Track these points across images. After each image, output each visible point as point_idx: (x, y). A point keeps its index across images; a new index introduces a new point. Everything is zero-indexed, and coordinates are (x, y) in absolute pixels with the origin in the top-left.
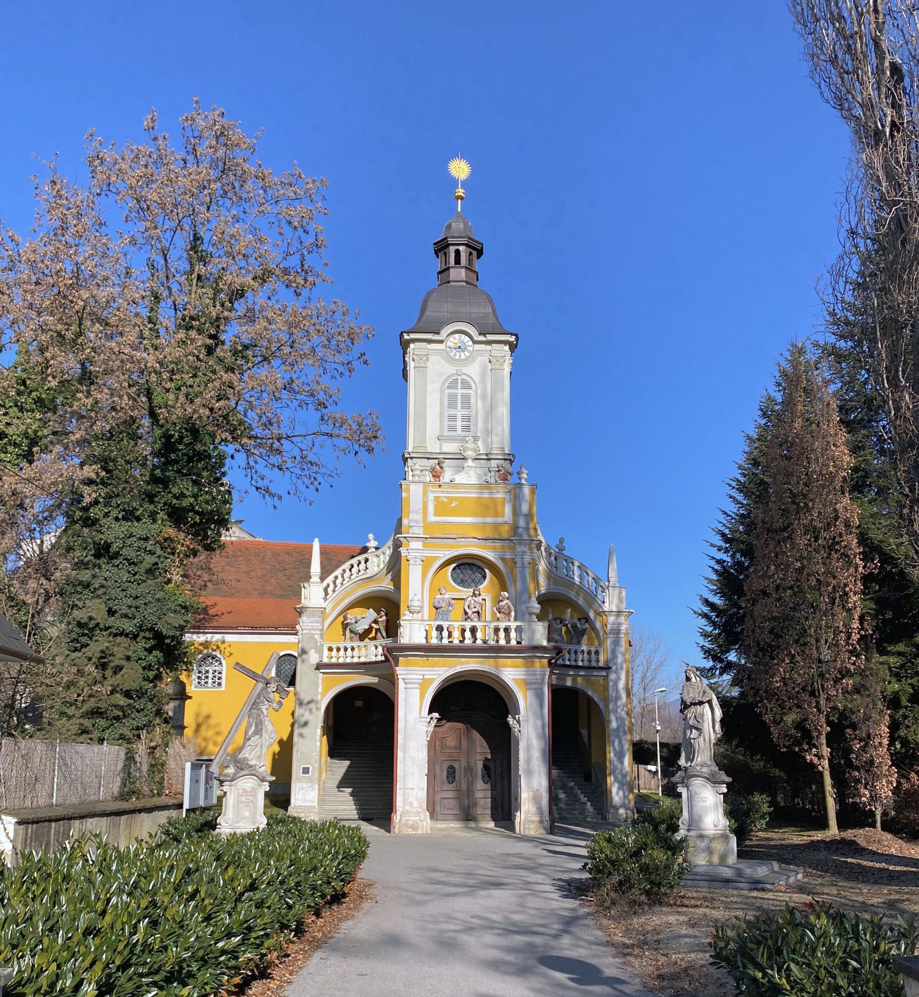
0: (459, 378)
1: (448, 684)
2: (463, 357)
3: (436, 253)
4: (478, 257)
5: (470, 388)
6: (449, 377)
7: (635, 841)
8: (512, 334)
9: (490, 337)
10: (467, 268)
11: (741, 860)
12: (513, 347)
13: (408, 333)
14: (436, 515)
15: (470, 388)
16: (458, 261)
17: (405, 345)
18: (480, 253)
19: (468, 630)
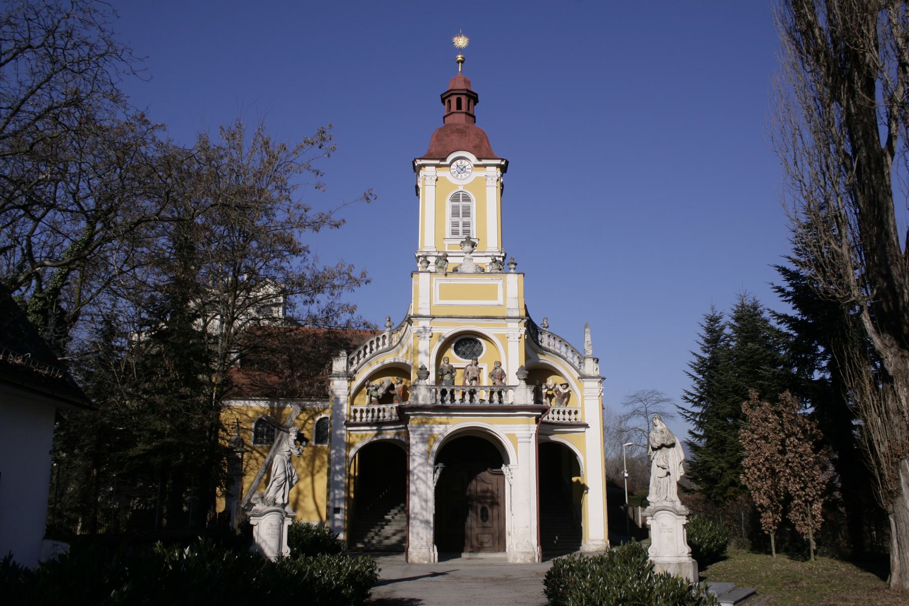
8: (503, 160)
16: (459, 106)
18: (476, 101)
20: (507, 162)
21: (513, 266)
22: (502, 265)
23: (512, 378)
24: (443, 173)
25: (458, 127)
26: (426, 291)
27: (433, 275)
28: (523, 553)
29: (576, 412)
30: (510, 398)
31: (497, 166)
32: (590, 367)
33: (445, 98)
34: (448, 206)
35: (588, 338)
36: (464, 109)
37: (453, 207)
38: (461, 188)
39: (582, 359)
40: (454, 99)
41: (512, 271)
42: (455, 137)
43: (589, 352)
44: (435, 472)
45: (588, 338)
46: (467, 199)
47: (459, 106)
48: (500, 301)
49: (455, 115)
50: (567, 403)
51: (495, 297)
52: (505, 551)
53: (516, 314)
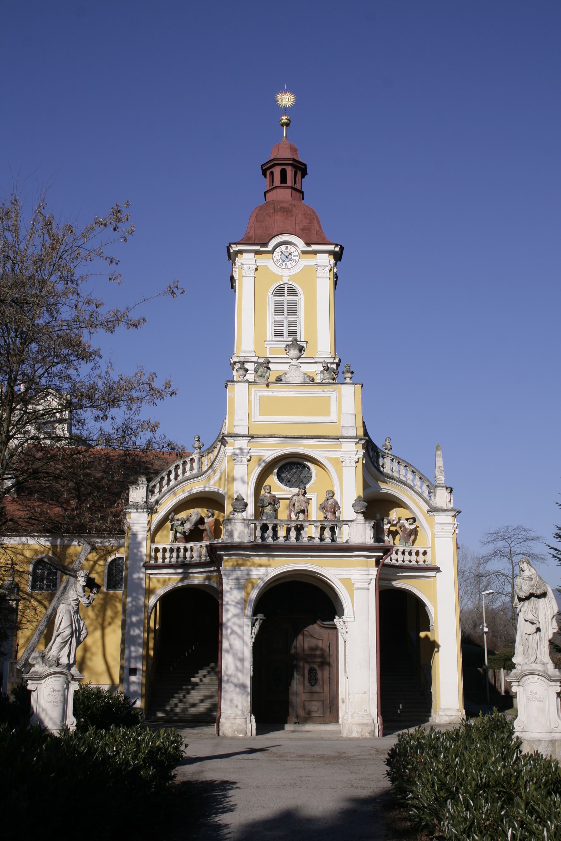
0: (286, 286)
1: (268, 588)
2: (289, 266)
3: (264, 173)
4: (303, 177)
5: (296, 295)
6: (273, 160)
7: (519, 783)
8: (336, 245)
9: (314, 248)
10: (293, 188)
11: (199, 517)
12: (338, 256)
13: (236, 244)
14: (261, 414)
15: (296, 295)
16: (284, 180)
17: (232, 257)
18: (304, 173)
19: (293, 529)
20: (342, 248)
21: (349, 375)
22: (336, 373)
23: (347, 511)
24: (263, 261)
25: (283, 205)
26: (244, 405)
27: (254, 389)
28: (359, 725)
29: (425, 553)
30: (345, 535)
31: (330, 253)
32: (442, 498)
33: (266, 170)
34: (271, 301)
35: (440, 462)
36: (290, 182)
37: (276, 302)
38: (285, 280)
39: (432, 488)
40: (277, 171)
41: (348, 380)
42: (278, 217)
43: (441, 480)
44: (253, 625)
45: (440, 462)
46: (293, 292)
47: (284, 180)
48: (333, 417)
49: (278, 190)
50: (414, 542)
51: (328, 414)
52: (337, 722)
53: (353, 433)
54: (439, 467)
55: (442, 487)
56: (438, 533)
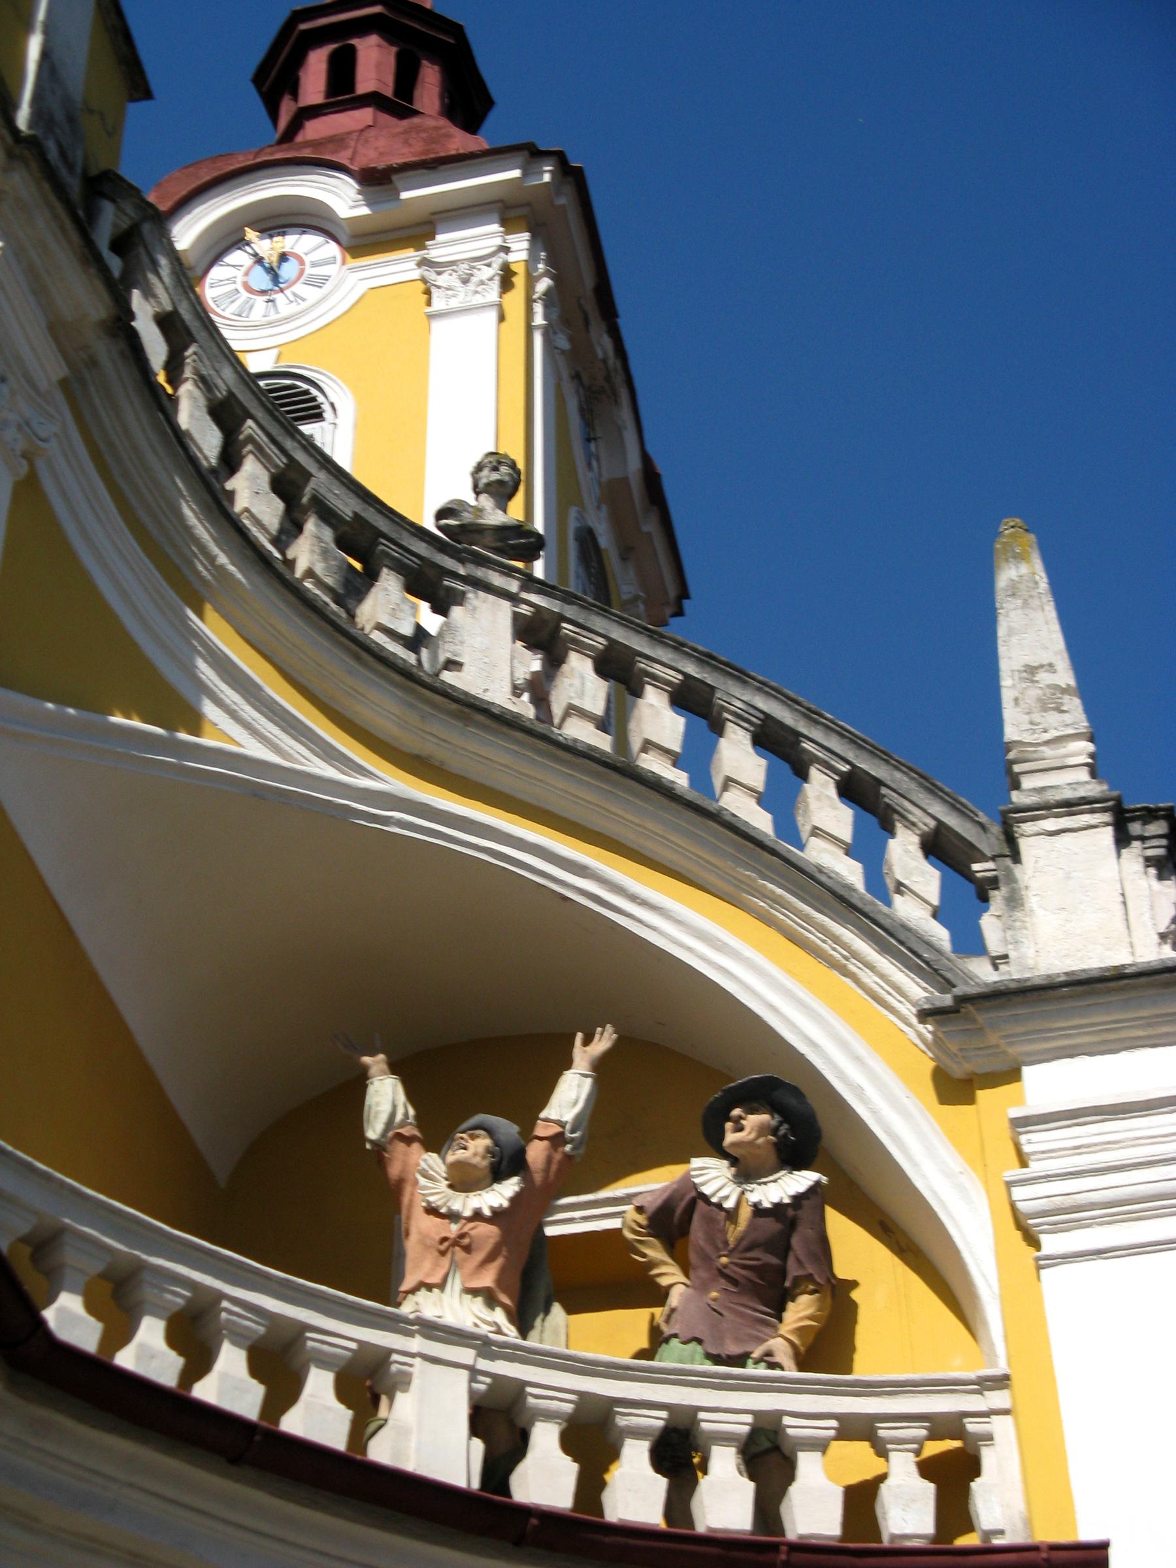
8: (533, 154)
20: (570, 174)
31: (509, 210)
54: (1031, 671)
55: (1070, 806)
56: (1071, 1215)
